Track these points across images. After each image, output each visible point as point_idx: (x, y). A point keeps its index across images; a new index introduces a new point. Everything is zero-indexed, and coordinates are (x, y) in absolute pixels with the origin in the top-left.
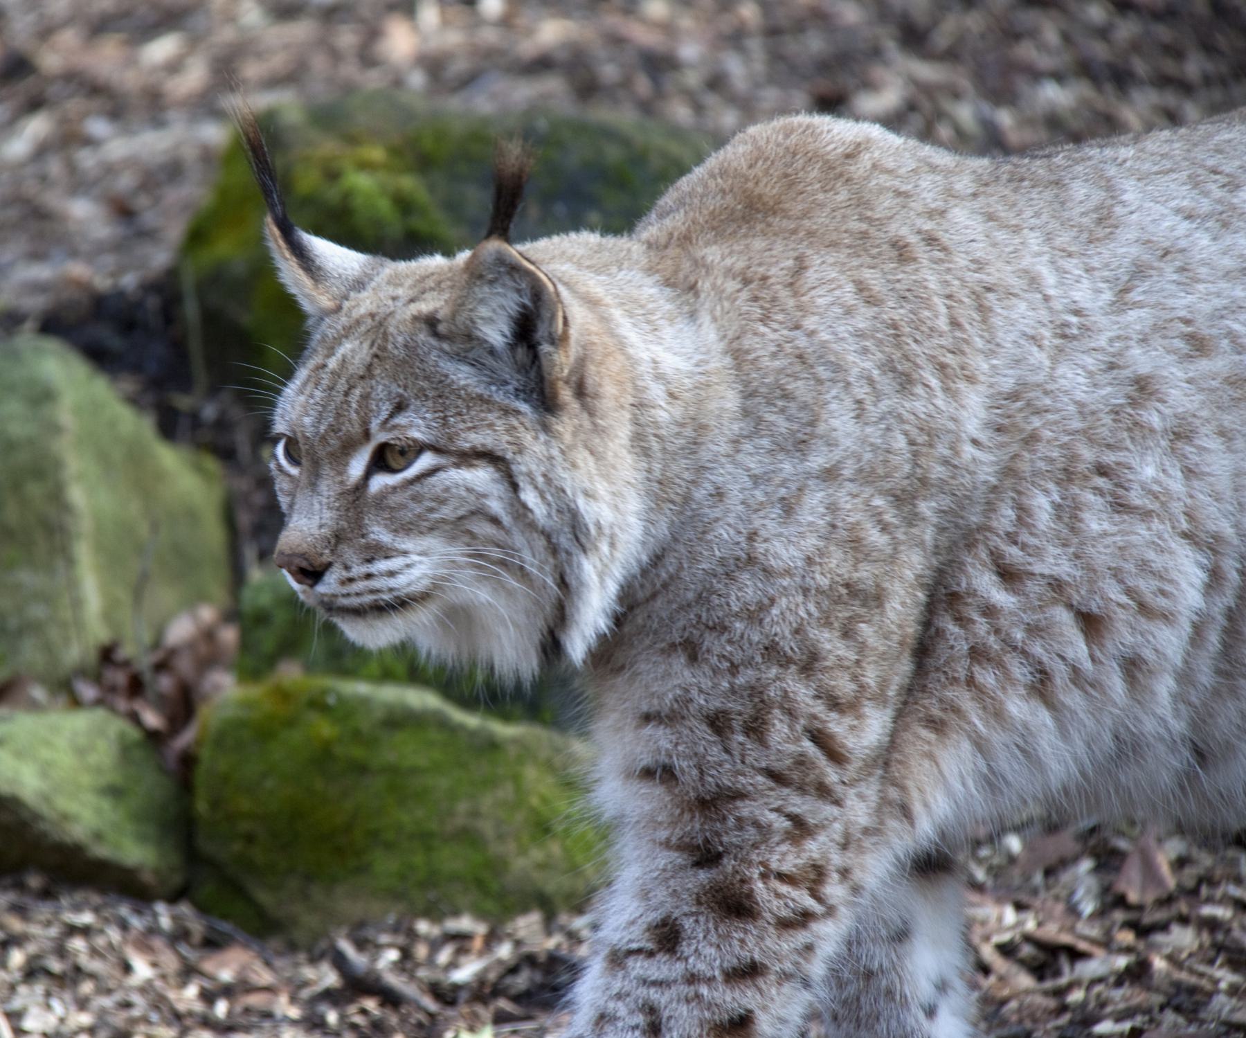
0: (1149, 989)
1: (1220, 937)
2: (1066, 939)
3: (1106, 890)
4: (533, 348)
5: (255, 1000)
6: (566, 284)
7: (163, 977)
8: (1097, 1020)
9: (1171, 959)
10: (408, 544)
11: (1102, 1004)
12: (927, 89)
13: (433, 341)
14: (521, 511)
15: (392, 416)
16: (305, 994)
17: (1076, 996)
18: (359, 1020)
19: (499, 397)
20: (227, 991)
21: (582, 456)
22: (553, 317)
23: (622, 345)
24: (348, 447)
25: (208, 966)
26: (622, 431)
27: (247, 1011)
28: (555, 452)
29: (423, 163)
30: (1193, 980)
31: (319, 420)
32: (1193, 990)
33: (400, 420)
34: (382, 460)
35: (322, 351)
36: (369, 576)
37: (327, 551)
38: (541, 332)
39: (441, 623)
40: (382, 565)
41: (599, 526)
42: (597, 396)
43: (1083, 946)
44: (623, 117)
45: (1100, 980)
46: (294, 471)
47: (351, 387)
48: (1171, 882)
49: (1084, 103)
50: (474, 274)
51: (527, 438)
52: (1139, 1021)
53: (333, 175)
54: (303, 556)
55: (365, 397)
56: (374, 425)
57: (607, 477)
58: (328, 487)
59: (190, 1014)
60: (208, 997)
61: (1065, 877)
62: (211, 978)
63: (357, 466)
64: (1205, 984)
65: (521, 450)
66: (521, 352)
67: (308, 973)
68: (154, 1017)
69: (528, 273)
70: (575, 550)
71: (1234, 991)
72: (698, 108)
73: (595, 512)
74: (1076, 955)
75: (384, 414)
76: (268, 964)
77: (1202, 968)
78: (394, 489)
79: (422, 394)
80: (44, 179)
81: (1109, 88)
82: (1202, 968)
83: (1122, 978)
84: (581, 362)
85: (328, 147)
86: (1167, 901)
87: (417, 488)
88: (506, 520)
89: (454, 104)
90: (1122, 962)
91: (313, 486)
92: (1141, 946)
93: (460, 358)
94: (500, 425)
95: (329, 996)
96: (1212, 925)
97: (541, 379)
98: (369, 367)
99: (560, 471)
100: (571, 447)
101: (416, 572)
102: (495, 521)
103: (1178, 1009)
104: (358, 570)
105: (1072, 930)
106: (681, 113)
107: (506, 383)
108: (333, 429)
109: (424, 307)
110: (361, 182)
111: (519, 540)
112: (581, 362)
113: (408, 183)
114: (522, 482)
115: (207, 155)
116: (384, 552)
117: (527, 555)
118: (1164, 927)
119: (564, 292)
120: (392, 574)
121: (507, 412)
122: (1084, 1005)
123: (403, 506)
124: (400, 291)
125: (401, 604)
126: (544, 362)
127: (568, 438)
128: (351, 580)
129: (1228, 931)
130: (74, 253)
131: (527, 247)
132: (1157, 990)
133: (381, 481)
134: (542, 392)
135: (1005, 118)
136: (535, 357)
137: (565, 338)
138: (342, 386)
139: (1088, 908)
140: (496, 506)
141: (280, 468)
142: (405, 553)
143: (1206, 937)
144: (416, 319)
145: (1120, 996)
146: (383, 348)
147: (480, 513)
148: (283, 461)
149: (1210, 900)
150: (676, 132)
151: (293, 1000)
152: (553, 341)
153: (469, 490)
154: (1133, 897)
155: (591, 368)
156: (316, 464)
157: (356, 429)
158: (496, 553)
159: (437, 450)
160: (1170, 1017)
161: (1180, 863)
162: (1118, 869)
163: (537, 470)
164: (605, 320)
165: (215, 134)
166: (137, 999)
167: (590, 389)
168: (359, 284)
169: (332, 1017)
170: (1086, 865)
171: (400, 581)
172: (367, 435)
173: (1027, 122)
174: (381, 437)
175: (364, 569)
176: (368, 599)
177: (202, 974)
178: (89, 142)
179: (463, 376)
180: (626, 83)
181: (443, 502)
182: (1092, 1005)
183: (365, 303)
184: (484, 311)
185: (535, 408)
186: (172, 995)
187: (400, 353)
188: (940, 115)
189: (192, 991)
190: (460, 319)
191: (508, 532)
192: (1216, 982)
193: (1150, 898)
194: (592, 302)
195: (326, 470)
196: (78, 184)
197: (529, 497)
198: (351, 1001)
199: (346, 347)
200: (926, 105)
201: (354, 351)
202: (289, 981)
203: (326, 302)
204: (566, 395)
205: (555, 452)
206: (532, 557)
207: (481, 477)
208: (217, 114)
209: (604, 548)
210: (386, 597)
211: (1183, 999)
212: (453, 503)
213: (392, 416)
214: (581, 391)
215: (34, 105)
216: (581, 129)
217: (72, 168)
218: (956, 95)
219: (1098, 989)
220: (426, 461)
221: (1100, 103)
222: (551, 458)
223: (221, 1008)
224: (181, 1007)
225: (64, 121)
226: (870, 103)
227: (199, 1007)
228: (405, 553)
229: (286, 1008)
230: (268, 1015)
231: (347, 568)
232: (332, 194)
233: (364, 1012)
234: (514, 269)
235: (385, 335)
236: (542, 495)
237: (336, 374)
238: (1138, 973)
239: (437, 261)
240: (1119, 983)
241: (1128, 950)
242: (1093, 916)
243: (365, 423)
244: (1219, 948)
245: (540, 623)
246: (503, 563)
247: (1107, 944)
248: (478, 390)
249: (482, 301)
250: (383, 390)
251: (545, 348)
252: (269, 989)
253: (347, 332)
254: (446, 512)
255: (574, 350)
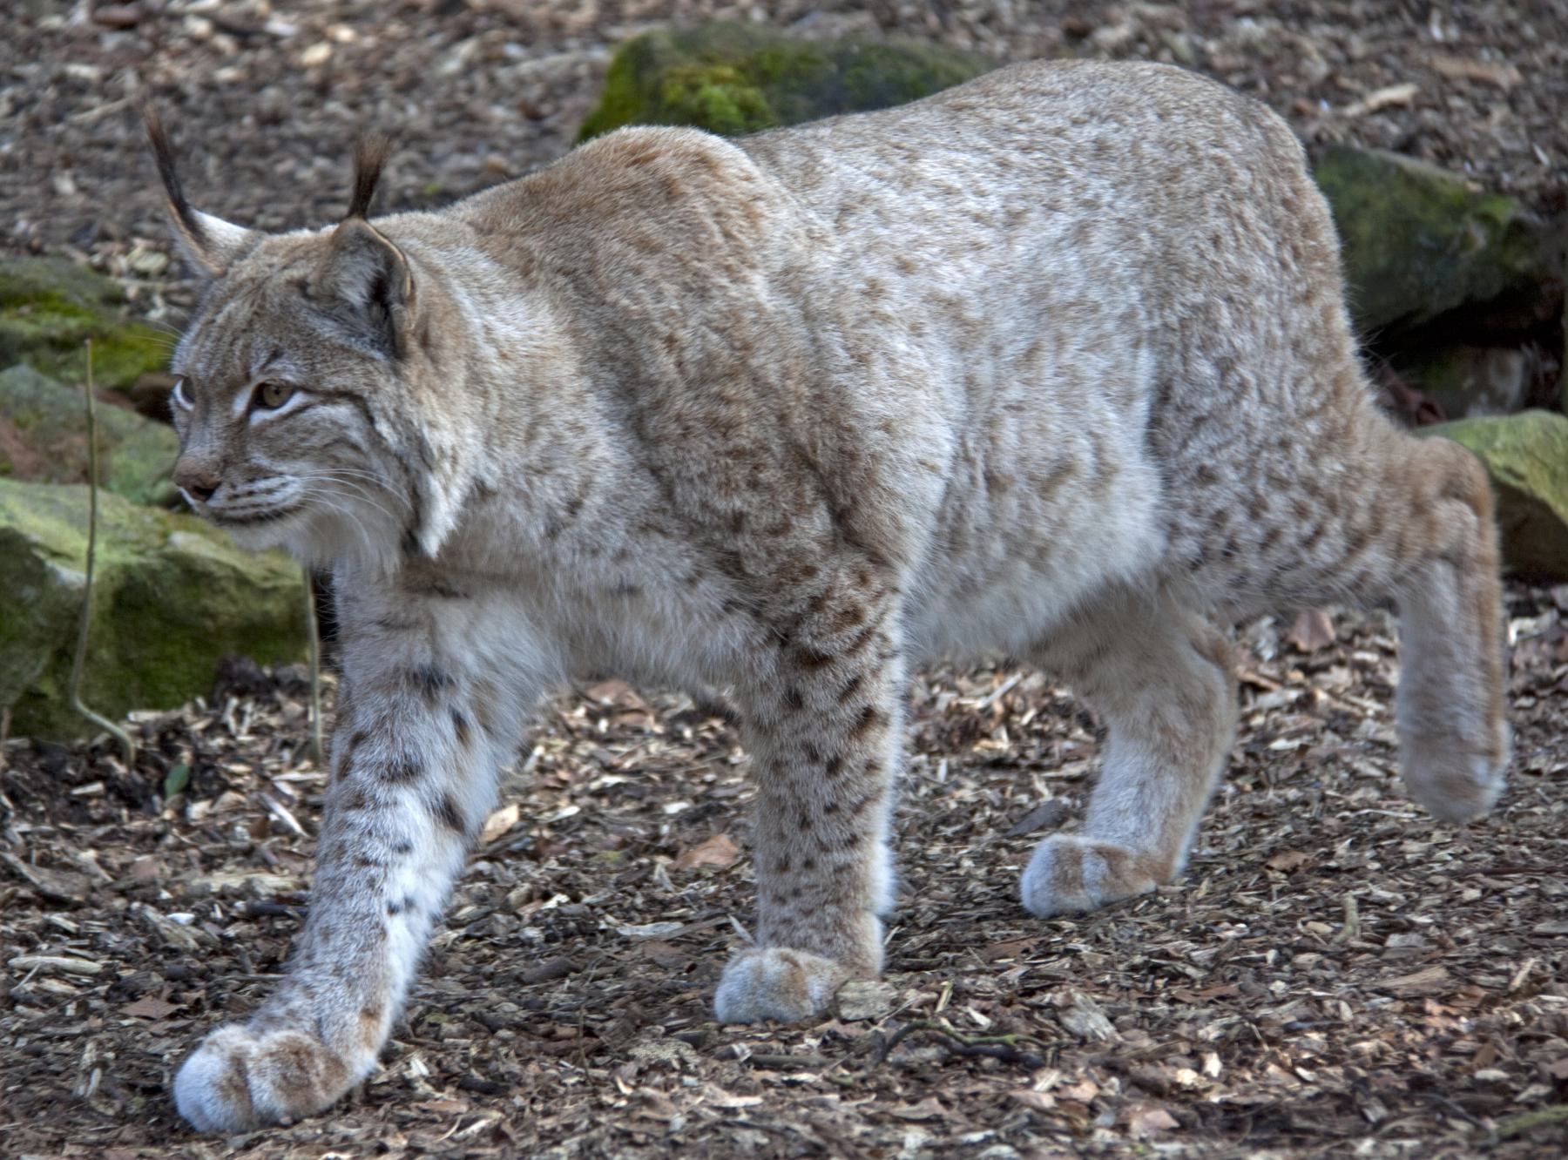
0: (1314, 715)
1: (1369, 676)
2: (1251, 677)
3: (1282, 640)
4: (385, 306)
5: (628, 719)
6: (414, 256)
7: (559, 701)
8: (1273, 738)
9: (1331, 692)
10: (283, 468)
11: (1278, 726)
12: (1152, 24)
13: (304, 301)
14: (377, 439)
15: (269, 362)
16: (667, 715)
17: (1258, 721)
18: (708, 735)
19: (358, 347)
20: (608, 712)
21: (426, 395)
22: (402, 283)
23: (457, 308)
24: (233, 388)
25: (593, 694)
26: (460, 376)
27: (623, 727)
28: (404, 392)
29: (763, 78)
30: (1348, 708)
31: (209, 365)
32: (1347, 716)
33: (276, 365)
34: (261, 399)
35: (211, 309)
36: (251, 493)
37: (784, 791)
38: (392, 294)
39: (312, 530)
40: (262, 484)
41: (441, 449)
42: (438, 347)
43: (1263, 682)
44: (918, 44)
45: (1277, 709)
46: (190, 407)
47: (236, 339)
48: (1332, 634)
49: (1272, 32)
50: (338, 245)
51: (381, 380)
52: (1306, 739)
53: (694, 88)
54: (197, 476)
55: (247, 347)
56: (254, 369)
57: (448, 411)
58: (217, 421)
59: (579, 729)
60: (593, 716)
61: (1251, 630)
62: (595, 702)
63: (240, 404)
64: (1356, 711)
65: (376, 390)
66: (376, 309)
67: (670, 699)
68: (552, 731)
69: (383, 246)
70: (423, 469)
71: (1378, 717)
72: (976, 38)
73: (441, 438)
74: (1258, 689)
75: (262, 361)
76: (638, 692)
77: (1355, 699)
78: (272, 423)
79: (294, 344)
80: (471, 91)
81: (1293, 25)
82: (1355, 699)
83: (1292, 707)
84: (425, 318)
85: (689, 65)
86: (1329, 648)
87: (290, 422)
88: (365, 446)
89: (789, 32)
90: (1293, 695)
91: (205, 419)
92: (1308, 682)
93: (325, 314)
94: (358, 370)
95: (688, 718)
96: (1362, 666)
97: (392, 331)
98: (250, 323)
99: (408, 408)
100: (417, 388)
101: (290, 490)
102: (355, 447)
103: (1336, 731)
104: (243, 488)
105: (1255, 671)
106: (962, 41)
107: (362, 335)
108: (221, 373)
109: (296, 273)
110: (716, 92)
111: (376, 462)
112: (425, 318)
113: (751, 93)
114: (377, 416)
115: (596, 73)
116: (265, 474)
117: (384, 477)
118: (1325, 669)
119: (411, 262)
120: (270, 491)
121: (364, 359)
122: (1263, 728)
123: (279, 437)
124: (275, 260)
125: (279, 515)
126: (396, 319)
127: (414, 380)
128: (236, 496)
129: (1374, 672)
130: (494, 148)
131: (378, 223)
132: (1320, 716)
133: (260, 416)
134: (393, 343)
135: (1212, 46)
136: (387, 313)
137: (412, 298)
138: (227, 338)
139: (1268, 654)
140: (355, 436)
141: (178, 404)
142: (281, 474)
143: (1358, 676)
144: (289, 282)
145: (1292, 721)
146: (261, 307)
147: (343, 441)
148: (181, 399)
149: (1361, 648)
150: (960, 56)
151: (658, 720)
152: (402, 301)
153: (334, 423)
154: (1303, 645)
155: (434, 324)
156: (207, 402)
157: (239, 373)
158: (357, 474)
159: (307, 390)
160: (1329, 737)
161: (1339, 620)
162: (1292, 624)
163: (390, 408)
164: (444, 286)
165: (602, 56)
166: (540, 718)
167: (433, 341)
168: (242, 253)
169: (688, 733)
170: (1267, 621)
171: (278, 497)
172: (248, 378)
173: (1228, 50)
174: (261, 379)
175: (247, 488)
176: (251, 511)
177: (589, 699)
178: (507, 62)
179: (328, 330)
180: (921, 19)
181: (312, 433)
182: (1270, 727)
183: (246, 269)
184: (346, 276)
185: (387, 356)
186: (566, 715)
187: (276, 311)
188: (1163, 45)
189: (581, 712)
190: (328, 282)
191: (366, 455)
192: (1364, 709)
193: (1315, 646)
194: (434, 272)
195: (215, 407)
196: (498, 94)
197: (383, 428)
198: (702, 721)
199: (231, 306)
200: (1151, 37)
201: (238, 309)
202: (655, 706)
203: (214, 268)
204: (413, 345)
205: (404, 392)
206: (389, 479)
207: (342, 412)
208: (606, 41)
209: (447, 466)
210: (266, 510)
211: (1340, 723)
212: (320, 434)
213: (269, 362)
214: (425, 342)
215: (465, 33)
216: (887, 52)
217: (492, 80)
218: (1176, 30)
219: (1276, 715)
220: (298, 399)
221: (1287, 36)
222: (400, 397)
223: (603, 725)
224: (572, 724)
225: (485, 46)
226: (1109, 36)
227: (586, 724)
228: (281, 474)
229: (652, 725)
230: (639, 731)
231: (233, 486)
232: (693, 102)
233: (712, 729)
234: (371, 242)
235: (264, 296)
236: (393, 426)
237: (223, 328)
238: (1306, 703)
239: (305, 234)
240: (1291, 711)
241: (1298, 686)
242: (1272, 660)
243: (246, 368)
244: (1367, 684)
245: (399, 526)
246: (363, 481)
247: (1282, 681)
248: (340, 342)
249: (344, 268)
250: (261, 342)
251: (396, 306)
252: (639, 711)
253: (232, 293)
254: (315, 441)
255: (419, 308)
